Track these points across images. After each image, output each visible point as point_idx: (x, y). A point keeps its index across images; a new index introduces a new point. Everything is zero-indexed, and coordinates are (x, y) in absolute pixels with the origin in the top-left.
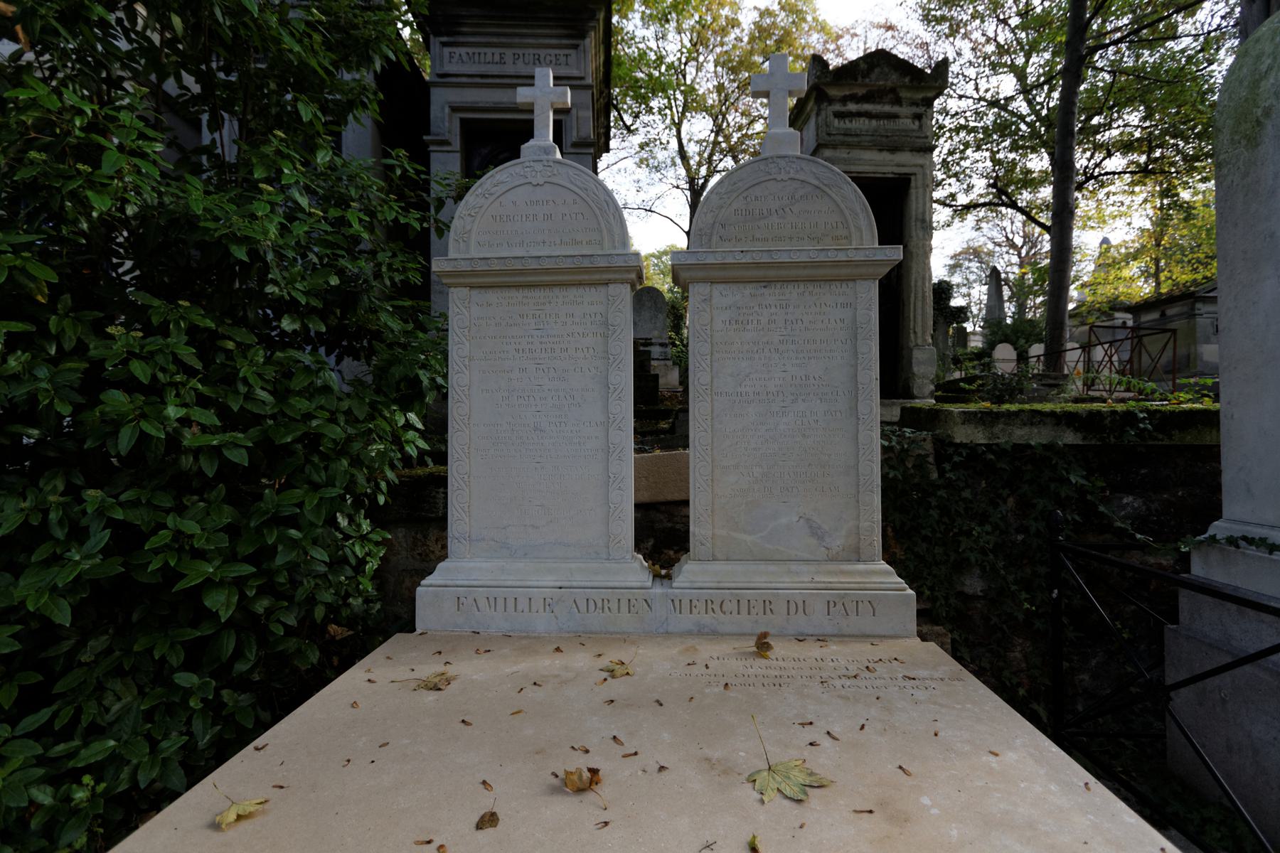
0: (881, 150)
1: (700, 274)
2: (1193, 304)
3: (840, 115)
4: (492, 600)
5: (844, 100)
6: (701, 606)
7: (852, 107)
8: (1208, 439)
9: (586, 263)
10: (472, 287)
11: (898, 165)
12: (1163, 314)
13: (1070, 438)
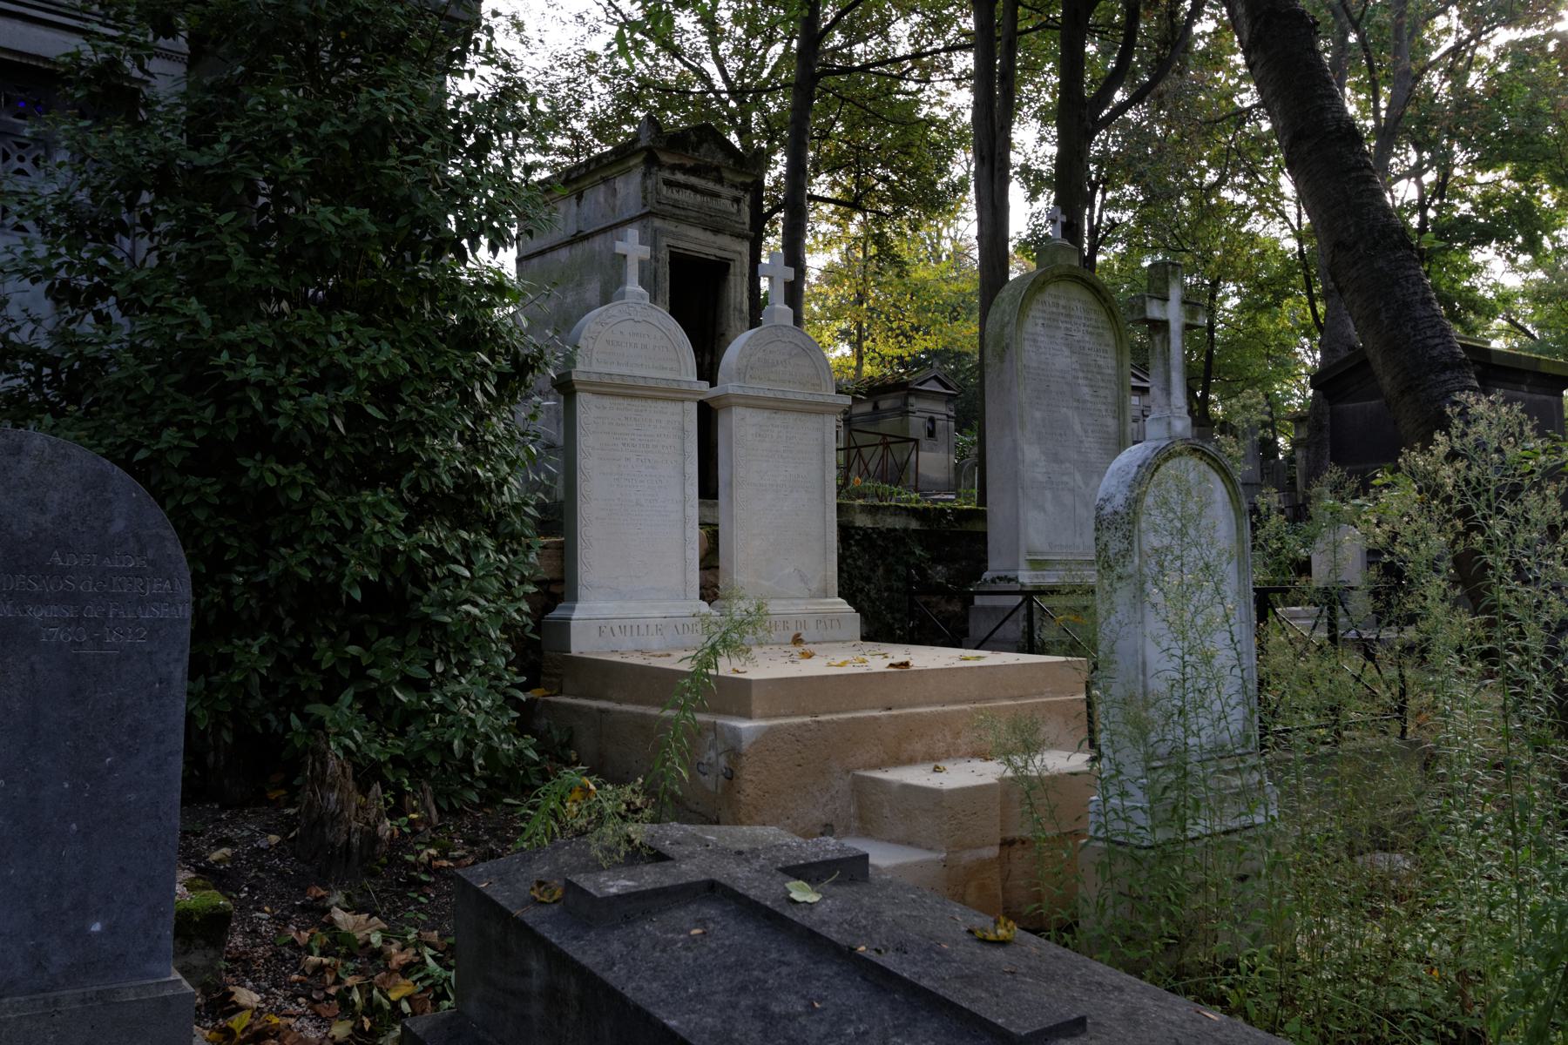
2: (906, 398)
3: (669, 183)
5: (674, 168)
7: (680, 177)
8: (979, 527)
9: (675, 386)
10: (594, 393)
12: (876, 407)
13: (914, 525)
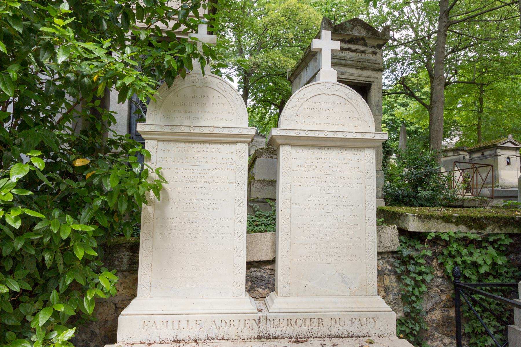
0: (357, 68)
1: (287, 141)
4: (165, 322)
6: (285, 322)
10: (159, 140)
11: (365, 77)
12: (483, 154)
